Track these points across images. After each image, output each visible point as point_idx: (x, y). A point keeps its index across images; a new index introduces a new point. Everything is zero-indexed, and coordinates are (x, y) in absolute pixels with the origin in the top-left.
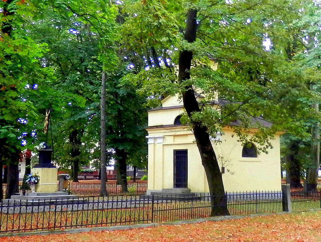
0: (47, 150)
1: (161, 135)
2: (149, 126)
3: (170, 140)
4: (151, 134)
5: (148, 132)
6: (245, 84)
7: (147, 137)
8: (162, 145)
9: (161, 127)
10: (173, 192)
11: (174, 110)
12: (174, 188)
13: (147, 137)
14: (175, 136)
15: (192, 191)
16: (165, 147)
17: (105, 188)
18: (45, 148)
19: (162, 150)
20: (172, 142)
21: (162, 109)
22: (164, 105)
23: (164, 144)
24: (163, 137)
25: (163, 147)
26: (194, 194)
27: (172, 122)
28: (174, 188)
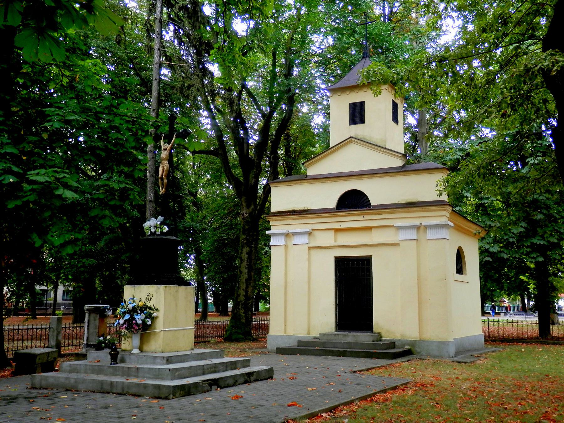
0: (169, 237)
1: (307, 229)
2: (272, 210)
3: (328, 239)
4: (277, 227)
5: (271, 223)
6: (491, 205)
7: (268, 232)
8: (306, 247)
9: (305, 212)
10: (334, 339)
11: (340, 180)
12: (336, 331)
13: (268, 232)
14: (337, 230)
15: (387, 337)
16: (312, 252)
17: (93, 345)
18: (167, 233)
19: (306, 257)
20: (332, 243)
21: (306, 178)
22: (310, 172)
23: (310, 245)
24: (310, 234)
25: (309, 252)
26: (392, 345)
27: (332, 203)
28: (336, 331)
